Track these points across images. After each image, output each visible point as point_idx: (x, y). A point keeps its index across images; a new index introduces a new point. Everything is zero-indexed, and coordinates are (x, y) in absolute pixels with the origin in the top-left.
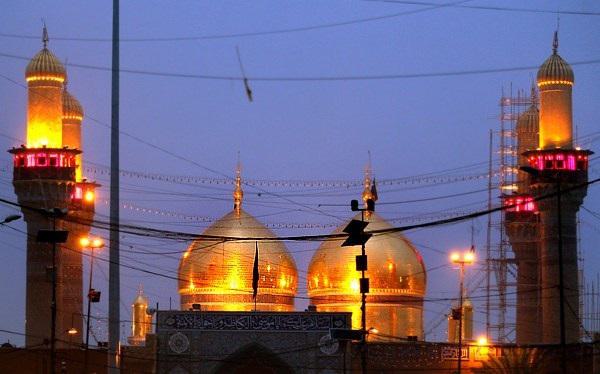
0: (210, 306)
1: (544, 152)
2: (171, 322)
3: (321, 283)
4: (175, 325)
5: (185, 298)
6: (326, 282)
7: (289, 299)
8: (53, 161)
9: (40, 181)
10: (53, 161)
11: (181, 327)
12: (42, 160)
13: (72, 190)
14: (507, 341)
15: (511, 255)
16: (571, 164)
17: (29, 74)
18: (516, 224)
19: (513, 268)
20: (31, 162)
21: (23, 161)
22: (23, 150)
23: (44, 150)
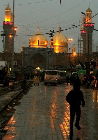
0: (34, 47)
1: (87, 23)
4: (26, 50)
5: (30, 45)
7: (46, 46)
8: (9, 24)
9: (7, 27)
10: (9, 24)
12: (7, 23)
14: (81, 53)
15: (82, 40)
16: (91, 25)
17: (5, 10)
18: (83, 35)
19: (82, 42)
21: (4, 23)
22: (4, 22)
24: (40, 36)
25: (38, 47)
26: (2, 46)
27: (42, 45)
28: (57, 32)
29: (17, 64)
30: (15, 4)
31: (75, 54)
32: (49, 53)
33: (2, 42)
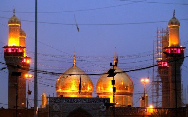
0: (66, 96)
1: (170, 48)
2: (53, 101)
3: (101, 89)
4: (55, 102)
5: (58, 93)
6: (102, 88)
7: (91, 94)
8: (17, 50)
9: (13, 57)
10: (17, 50)
11: (57, 102)
12: (13, 50)
13: (22, 59)
14: (159, 107)
15: (160, 80)
16: (179, 51)
17: (9, 23)
18: (162, 70)
19: (161, 84)
20: (10, 51)
21: (7, 50)
22: (7, 47)
23: (14, 47)
24: (33, 79)
30: (38, 21)
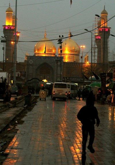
0: (40, 55)
1: (102, 28)
4: (30, 59)
5: (36, 54)
7: (54, 54)
8: (11, 28)
9: (8, 32)
10: (11, 28)
12: (8, 28)
14: (95, 63)
15: (96, 47)
16: (107, 30)
17: (6, 12)
18: (97, 41)
19: (97, 49)
21: (5, 28)
22: (5, 26)
25: (44, 55)
26: (3, 54)
27: (50, 53)
28: (66, 38)
29: (19, 76)
31: (88, 63)
32: (57, 62)
33: (3, 50)
